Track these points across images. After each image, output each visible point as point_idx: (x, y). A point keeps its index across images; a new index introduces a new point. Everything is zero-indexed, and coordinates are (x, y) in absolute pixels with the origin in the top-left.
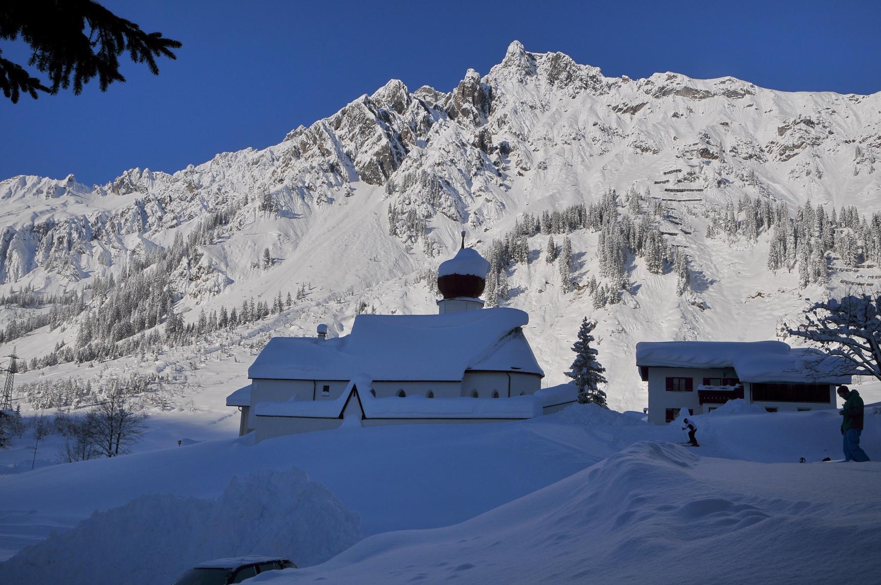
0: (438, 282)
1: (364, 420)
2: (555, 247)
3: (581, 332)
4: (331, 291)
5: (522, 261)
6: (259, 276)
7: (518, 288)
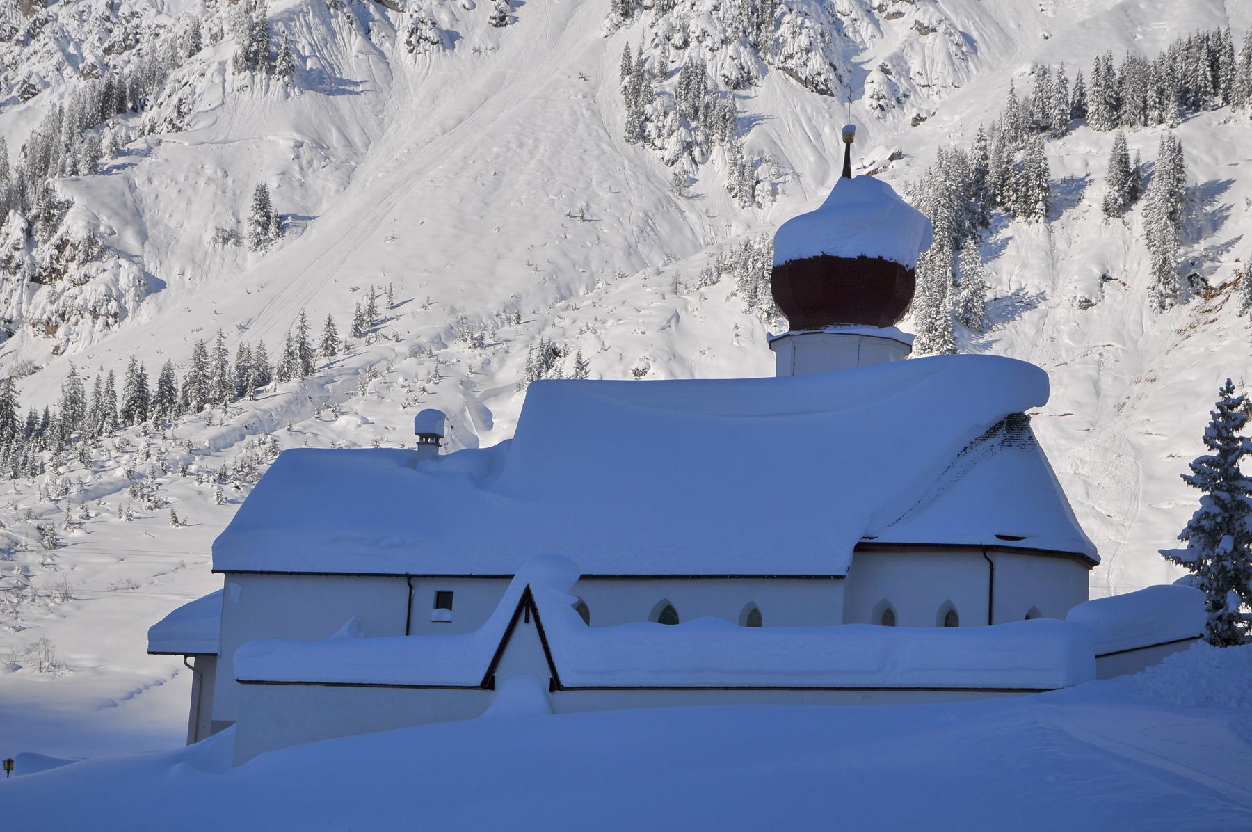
0: (773, 281)
1: (557, 693)
2: (1132, 166)
3: (1215, 425)
4: (453, 311)
5: (1028, 213)
6: (241, 269)
7: (1016, 294)
